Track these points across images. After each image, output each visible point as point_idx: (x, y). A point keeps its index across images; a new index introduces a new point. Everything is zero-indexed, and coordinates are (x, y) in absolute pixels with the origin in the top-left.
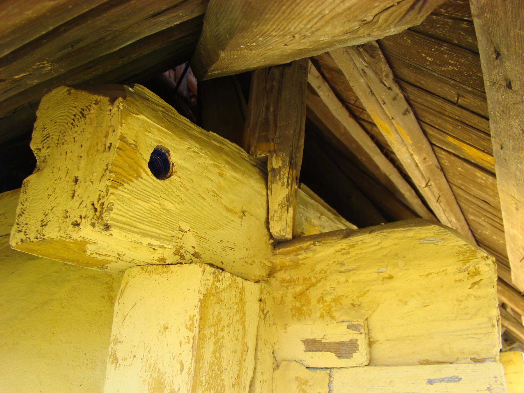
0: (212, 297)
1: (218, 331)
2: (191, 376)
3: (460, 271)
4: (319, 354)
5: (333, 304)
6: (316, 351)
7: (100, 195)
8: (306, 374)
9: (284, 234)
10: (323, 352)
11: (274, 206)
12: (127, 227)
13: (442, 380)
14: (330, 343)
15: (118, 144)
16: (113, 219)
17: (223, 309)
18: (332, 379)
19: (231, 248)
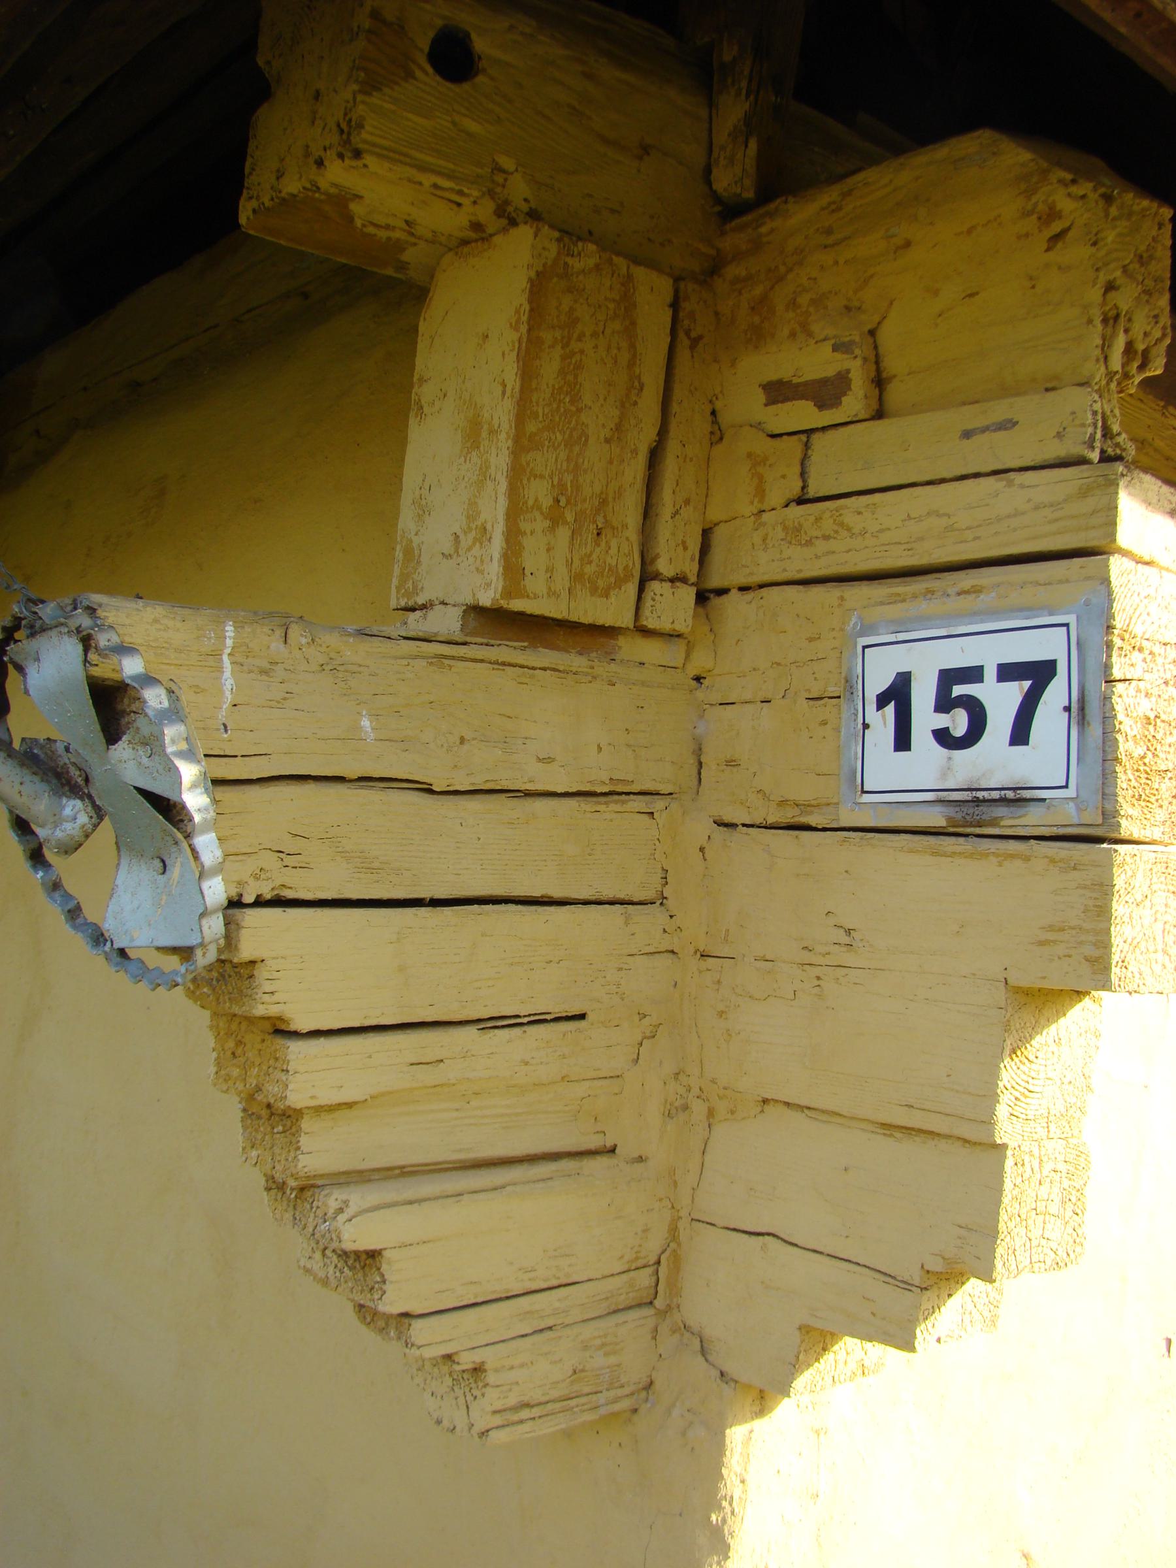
0: (555, 280)
1: (570, 339)
2: (514, 400)
3: (1026, 214)
4: (788, 405)
5: (812, 309)
6: (783, 402)
7: (346, 108)
8: (763, 445)
9: (739, 191)
10: (794, 402)
11: (721, 137)
12: (391, 154)
13: (985, 429)
14: (806, 384)
15: (367, 24)
16: (365, 142)
17: (582, 304)
18: (810, 452)
19: (613, 211)
